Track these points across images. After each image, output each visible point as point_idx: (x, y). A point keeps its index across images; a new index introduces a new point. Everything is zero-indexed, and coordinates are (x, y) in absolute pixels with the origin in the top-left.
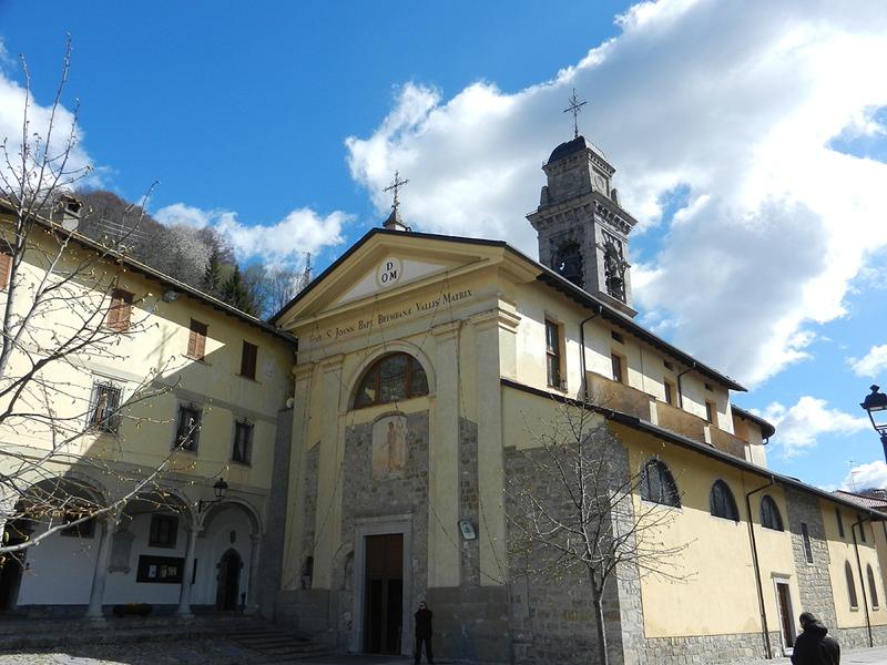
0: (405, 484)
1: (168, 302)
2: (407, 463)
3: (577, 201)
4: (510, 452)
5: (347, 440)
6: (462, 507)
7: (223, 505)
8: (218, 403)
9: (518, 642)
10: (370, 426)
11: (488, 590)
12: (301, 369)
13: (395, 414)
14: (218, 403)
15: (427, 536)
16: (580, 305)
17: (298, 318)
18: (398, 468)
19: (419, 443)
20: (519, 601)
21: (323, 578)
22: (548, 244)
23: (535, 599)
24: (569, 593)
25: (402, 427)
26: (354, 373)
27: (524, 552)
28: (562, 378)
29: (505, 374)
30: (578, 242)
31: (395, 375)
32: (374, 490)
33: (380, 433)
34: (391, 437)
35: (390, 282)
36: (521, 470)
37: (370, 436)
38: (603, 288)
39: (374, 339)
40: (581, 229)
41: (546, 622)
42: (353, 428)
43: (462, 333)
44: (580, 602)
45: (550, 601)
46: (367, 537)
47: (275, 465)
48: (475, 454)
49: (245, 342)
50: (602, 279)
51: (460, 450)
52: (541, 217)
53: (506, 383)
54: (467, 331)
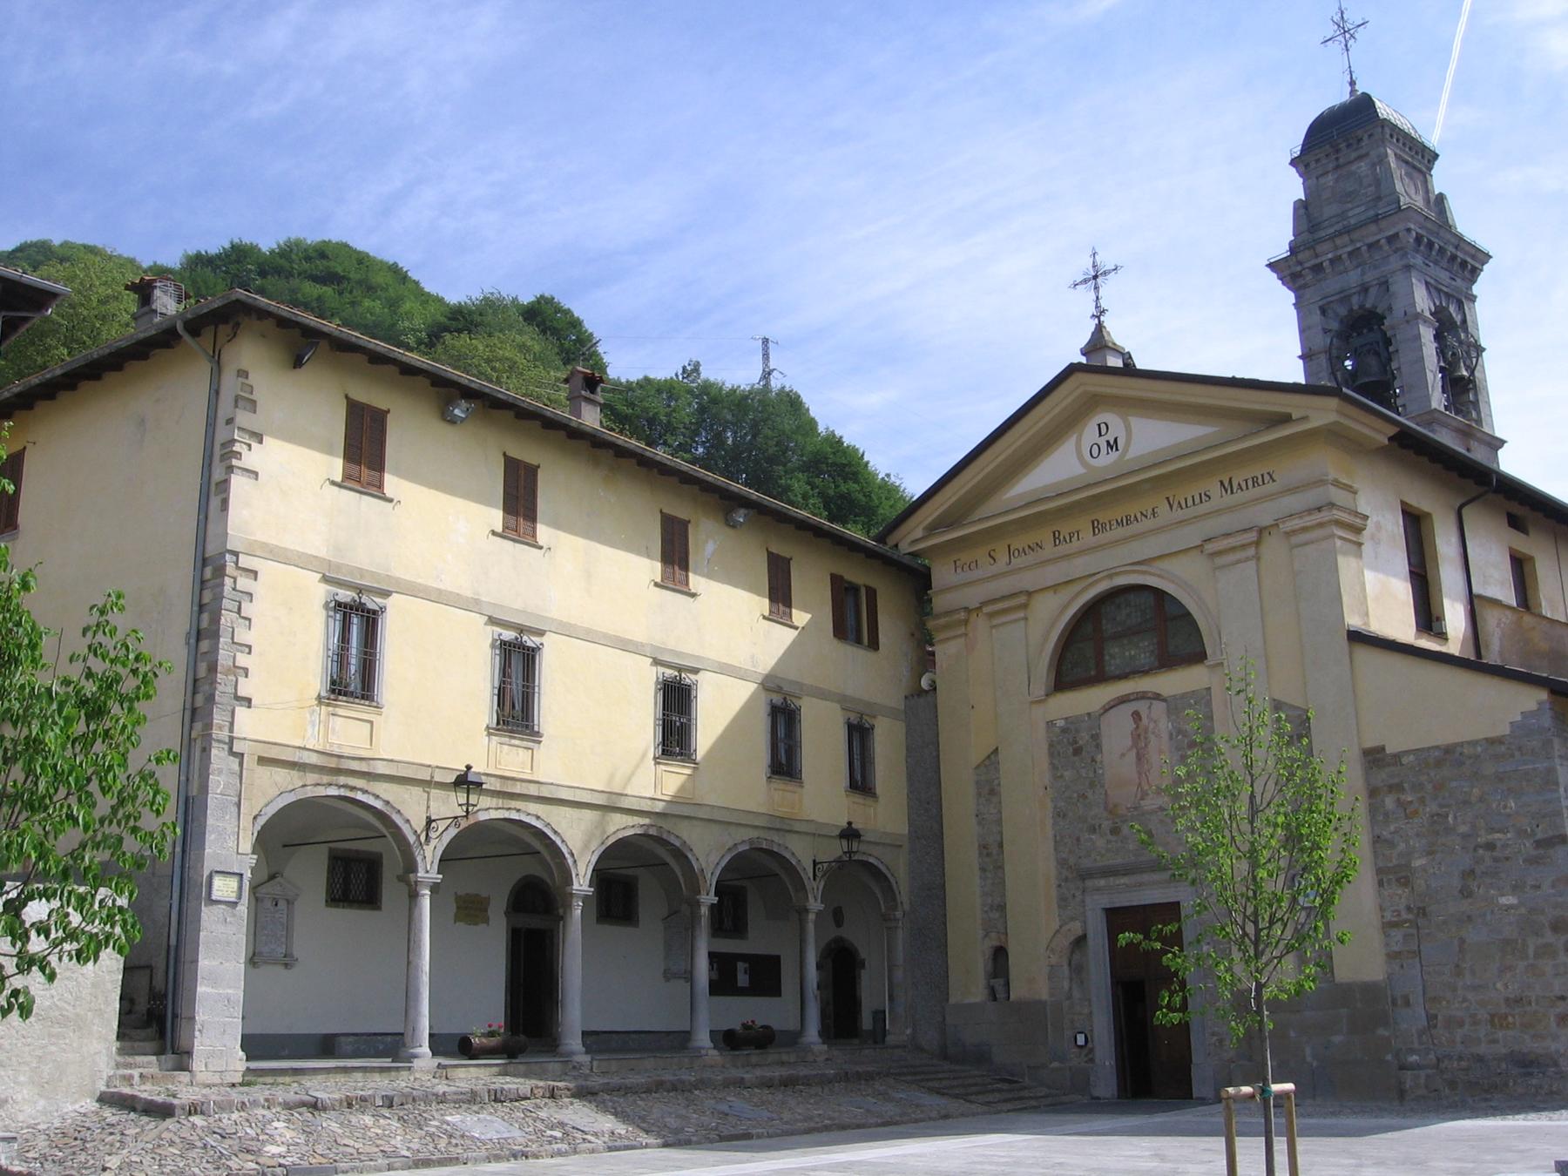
1: (734, 527)
3: (1373, 228)
4: (1374, 757)
5: (1051, 745)
7: (854, 870)
8: (822, 694)
9: (1412, 1067)
10: (1094, 719)
12: (942, 621)
13: (1142, 696)
14: (822, 694)
16: (1425, 460)
17: (932, 529)
18: (1159, 791)
19: (1197, 743)
20: (1407, 1003)
21: (1033, 976)
22: (1317, 317)
23: (1434, 999)
24: (1499, 985)
26: (1053, 625)
27: (1409, 924)
28: (1435, 612)
29: (1353, 621)
30: (1379, 311)
31: (1129, 630)
32: (1115, 831)
33: (1117, 733)
34: (1139, 737)
35: (1107, 459)
36: (1397, 788)
37: (1096, 737)
38: (1438, 400)
39: (1079, 566)
40: (1385, 285)
41: (1459, 1034)
42: (1061, 723)
43: (1264, 548)
44: (1518, 1001)
45: (1465, 1000)
47: (910, 792)
49: (770, 554)
50: (1434, 379)
52: (1300, 263)
53: (1358, 638)
54: (1273, 548)
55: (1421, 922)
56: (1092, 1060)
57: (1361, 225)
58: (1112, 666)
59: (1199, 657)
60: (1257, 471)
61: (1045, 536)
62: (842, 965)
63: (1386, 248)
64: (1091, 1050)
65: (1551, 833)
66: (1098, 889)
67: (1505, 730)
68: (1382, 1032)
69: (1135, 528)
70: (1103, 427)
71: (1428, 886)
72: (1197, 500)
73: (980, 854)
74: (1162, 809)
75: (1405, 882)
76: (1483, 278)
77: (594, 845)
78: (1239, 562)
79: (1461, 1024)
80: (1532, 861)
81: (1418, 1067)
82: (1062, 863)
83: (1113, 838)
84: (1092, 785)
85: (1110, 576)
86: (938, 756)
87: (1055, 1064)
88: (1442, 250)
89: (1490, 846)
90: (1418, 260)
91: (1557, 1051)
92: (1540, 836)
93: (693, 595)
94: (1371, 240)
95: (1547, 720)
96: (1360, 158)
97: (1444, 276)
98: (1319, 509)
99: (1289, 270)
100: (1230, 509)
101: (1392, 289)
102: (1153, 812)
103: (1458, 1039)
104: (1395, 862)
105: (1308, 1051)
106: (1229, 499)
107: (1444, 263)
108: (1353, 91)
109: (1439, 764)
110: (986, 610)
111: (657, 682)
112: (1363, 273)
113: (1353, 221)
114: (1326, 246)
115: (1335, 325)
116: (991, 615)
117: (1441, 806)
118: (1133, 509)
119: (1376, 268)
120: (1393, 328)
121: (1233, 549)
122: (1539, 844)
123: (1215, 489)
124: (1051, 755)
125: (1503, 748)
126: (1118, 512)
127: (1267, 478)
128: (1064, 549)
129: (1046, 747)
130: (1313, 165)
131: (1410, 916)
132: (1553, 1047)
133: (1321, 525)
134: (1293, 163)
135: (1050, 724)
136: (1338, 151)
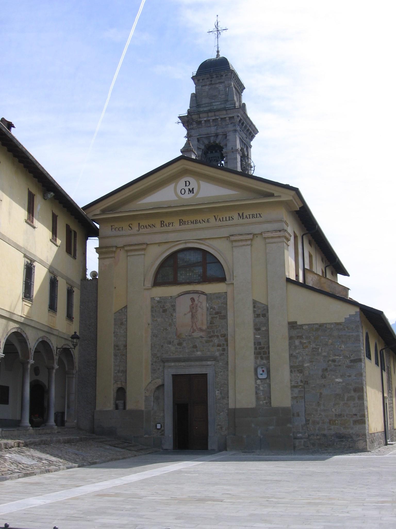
0: (207, 342)
2: (208, 328)
3: (224, 112)
4: (292, 325)
5: (152, 307)
6: (256, 358)
10: (173, 299)
11: (277, 411)
15: (228, 375)
17: (104, 211)
18: (201, 330)
19: (219, 313)
20: (298, 415)
21: (137, 399)
24: (333, 410)
25: (203, 303)
27: (301, 387)
30: (221, 145)
33: (183, 306)
34: (193, 309)
35: (188, 196)
36: (300, 337)
37: (173, 306)
39: (172, 237)
40: (225, 136)
42: (158, 299)
44: (340, 415)
46: (174, 376)
48: (266, 324)
51: (254, 321)
54: (258, 242)
55: (306, 386)
56: (163, 435)
57: (219, 110)
58: (181, 278)
59: (223, 279)
60: (255, 212)
61: (157, 222)
62: (39, 393)
63: (228, 121)
64: (163, 431)
65: (356, 358)
66: (170, 367)
67: (342, 320)
68: (289, 425)
69: (199, 225)
70: (188, 183)
71: (309, 373)
72: (228, 219)
73: (115, 349)
74: (202, 337)
75: (301, 371)
76: (254, 139)
77: (5, 335)
78: (244, 245)
79: (318, 423)
80: (348, 367)
81: (301, 438)
82: (154, 355)
83: (179, 347)
84: (170, 325)
85: (186, 243)
86: (96, 307)
87: (146, 436)
88: (246, 126)
89: (334, 361)
90: (238, 128)
91: (352, 433)
92: (352, 358)
93: (34, 228)
94: (223, 117)
95: (358, 319)
96: (221, 83)
97: (244, 136)
98: (280, 231)
99: (186, 121)
100: (241, 225)
101: (228, 138)
102: (197, 338)
103: (317, 429)
104: (297, 364)
105: (259, 432)
106: (241, 221)
107: (245, 131)
108: (218, 55)
109: (317, 330)
110: (126, 248)
111: (25, 265)
112: (217, 129)
113: (215, 107)
114: (204, 115)
115: (203, 147)
116: (127, 251)
117: (316, 345)
118: (199, 218)
119: (223, 128)
120: (226, 153)
121: (242, 240)
122: (351, 361)
123: (236, 216)
124: (152, 311)
125: (341, 327)
126: (192, 218)
127: (258, 216)
128: (165, 229)
129: (149, 308)
130: (201, 81)
131: (302, 384)
132: (351, 431)
133: (279, 237)
134: (193, 78)
135: (152, 299)
136: (212, 78)
